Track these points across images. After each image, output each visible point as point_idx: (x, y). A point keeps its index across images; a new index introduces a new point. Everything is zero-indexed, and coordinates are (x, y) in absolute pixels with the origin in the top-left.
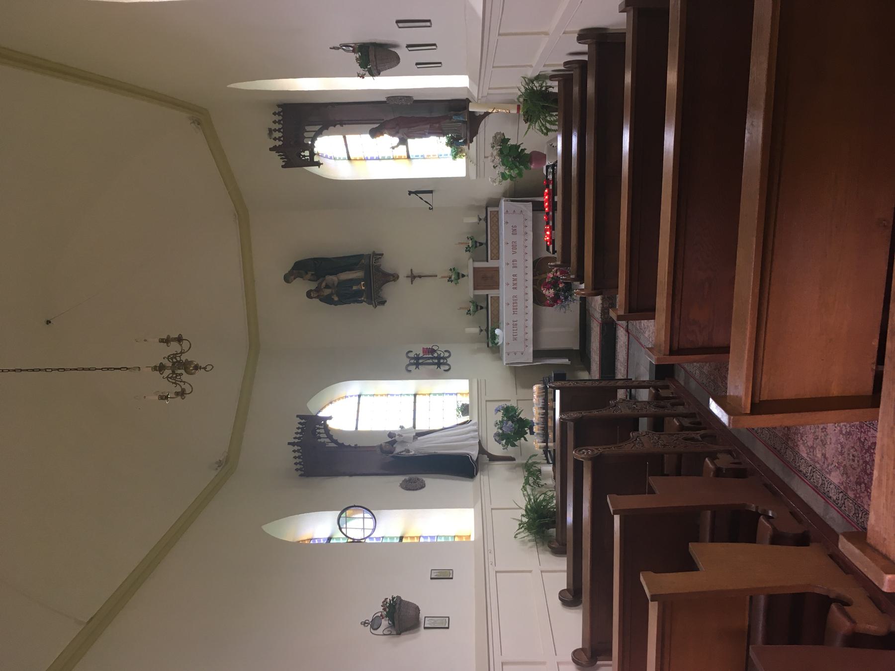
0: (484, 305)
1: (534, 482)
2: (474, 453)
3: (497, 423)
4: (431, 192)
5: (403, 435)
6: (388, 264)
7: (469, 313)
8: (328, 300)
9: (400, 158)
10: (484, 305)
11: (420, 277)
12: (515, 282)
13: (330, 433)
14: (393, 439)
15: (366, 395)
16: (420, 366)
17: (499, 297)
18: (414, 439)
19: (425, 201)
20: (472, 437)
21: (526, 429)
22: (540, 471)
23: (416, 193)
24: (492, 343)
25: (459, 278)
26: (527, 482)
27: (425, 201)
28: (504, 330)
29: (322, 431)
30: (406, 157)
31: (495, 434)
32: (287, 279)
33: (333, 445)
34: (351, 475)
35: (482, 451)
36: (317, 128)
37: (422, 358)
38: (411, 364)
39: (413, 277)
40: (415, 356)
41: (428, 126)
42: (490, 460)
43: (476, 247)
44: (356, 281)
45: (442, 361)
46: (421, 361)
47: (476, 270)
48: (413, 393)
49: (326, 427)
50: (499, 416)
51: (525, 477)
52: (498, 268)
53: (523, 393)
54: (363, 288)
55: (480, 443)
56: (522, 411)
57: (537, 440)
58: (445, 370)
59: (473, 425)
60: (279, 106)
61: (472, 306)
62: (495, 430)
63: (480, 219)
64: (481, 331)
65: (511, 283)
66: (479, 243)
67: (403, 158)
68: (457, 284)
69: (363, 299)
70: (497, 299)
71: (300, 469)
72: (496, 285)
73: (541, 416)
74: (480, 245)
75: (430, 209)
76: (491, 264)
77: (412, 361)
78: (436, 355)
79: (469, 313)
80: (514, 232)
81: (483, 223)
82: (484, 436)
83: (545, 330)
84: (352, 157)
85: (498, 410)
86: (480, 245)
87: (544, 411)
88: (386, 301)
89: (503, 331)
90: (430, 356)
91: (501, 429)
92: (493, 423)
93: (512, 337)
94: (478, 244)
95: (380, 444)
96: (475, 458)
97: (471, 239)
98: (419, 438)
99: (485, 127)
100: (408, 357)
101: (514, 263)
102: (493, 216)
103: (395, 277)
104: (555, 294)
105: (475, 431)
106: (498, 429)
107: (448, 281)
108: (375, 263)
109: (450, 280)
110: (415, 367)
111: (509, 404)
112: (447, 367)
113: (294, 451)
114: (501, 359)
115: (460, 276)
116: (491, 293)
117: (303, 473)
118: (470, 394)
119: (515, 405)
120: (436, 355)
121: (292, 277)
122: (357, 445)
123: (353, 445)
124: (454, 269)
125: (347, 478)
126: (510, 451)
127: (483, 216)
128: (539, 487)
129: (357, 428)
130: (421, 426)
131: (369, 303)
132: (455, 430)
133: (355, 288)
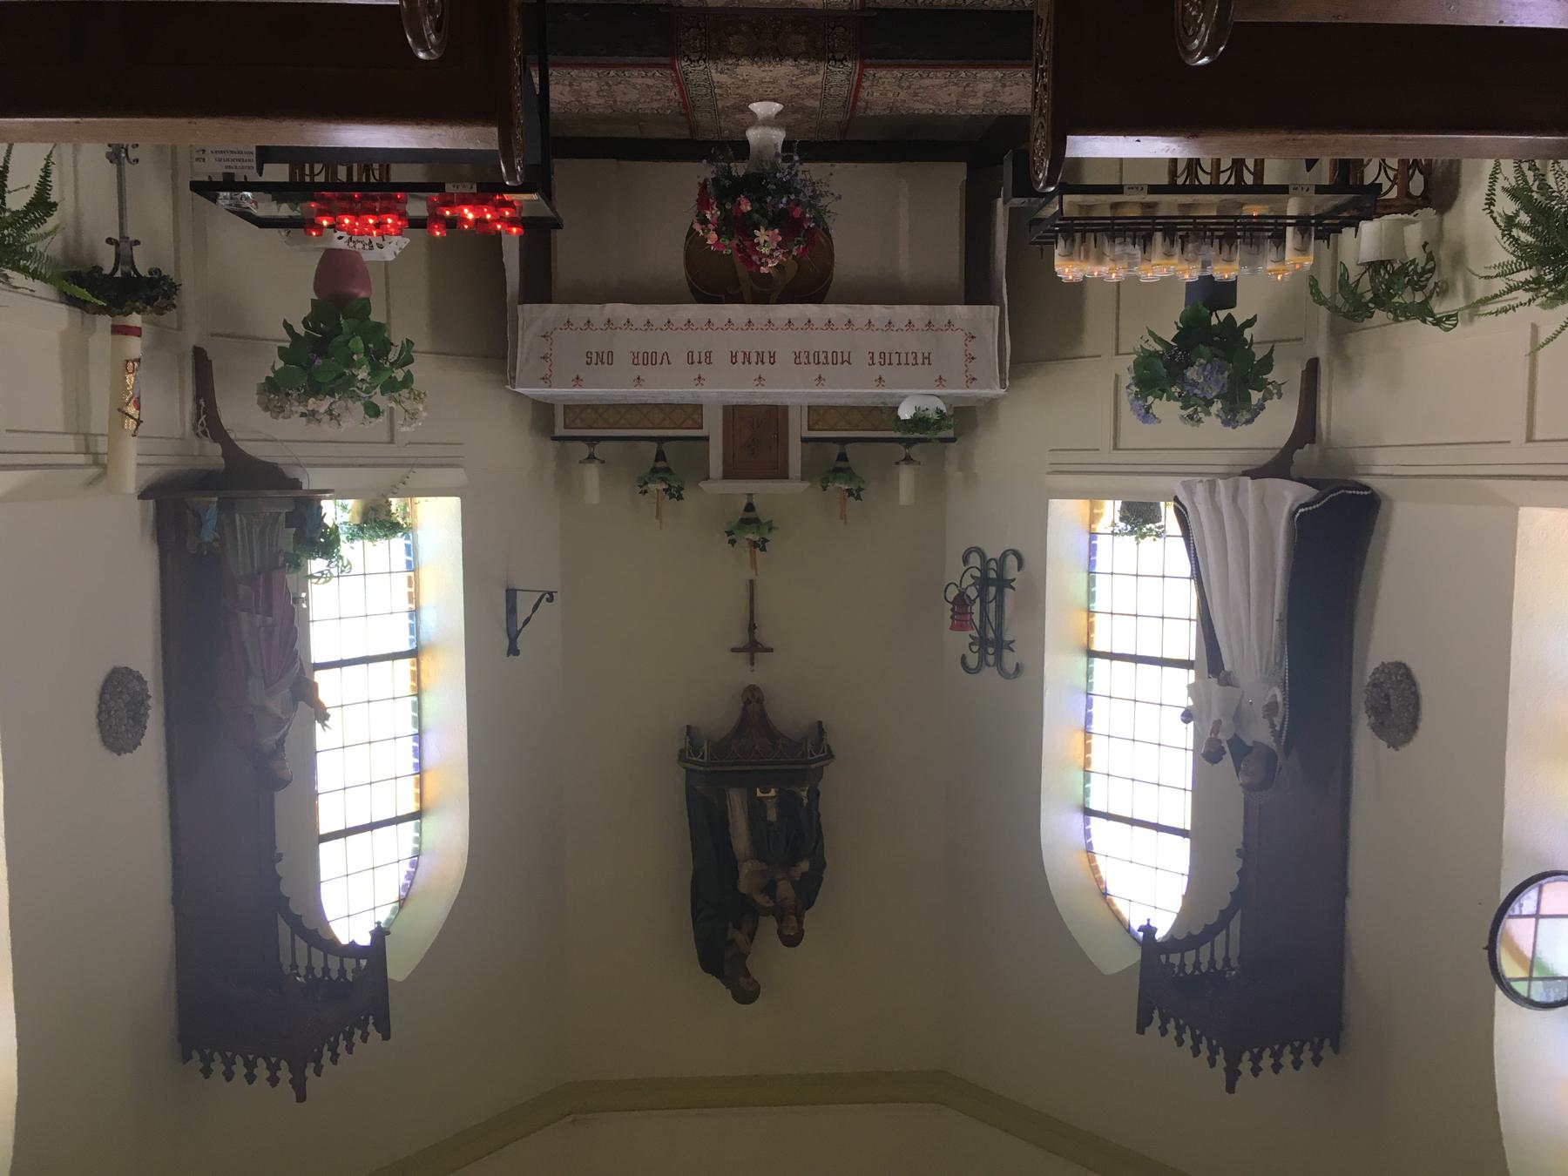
0: (835, 449)
1: (1417, 286)
2: (1290, 494)
3: (1191, 417)
4: (511, 594)
5: (1215, 717)
6: (718, 715)
7: (855, 494)
8: (808, 890)
9: (417, 676)
10: (835, 449)
11: (752, 628)
12: (754, 359)
13: (1196, 932)
14: (1227, 749)
15: (1086, 792)
16: (1007, 638)
17: (809, 407)
18: (1228, 684)
19: (533, 611)
20: (1234, 500)
21: (1214, 321)
22: (1374, 267)
23: (513, 637)
24: (939, 429)
25: (757, 521)
26: (1422, 312)
27: (533, 611)
28: (906, 391)
29: (1190, 957)
30: (414, 659)
31: (1226, 423)
32: (746, 994)
33: (1235, 924)
34: (1344, 892)
35: (1278, 467)
36: (284, 929)
37: (982, 631)
38: (999, 662)
39: (753, 648)
40: (975, 648)
41: (243, 615)
42: (1312, 442)
43: (667, 470)
44: (755, 809)
45: (993, 575)
46: (991, 635)
47: (728, 475)
48: (1084, 659)
49: (1172, 943)
50: (1167, 409)
51: (1396, 320)
52: (726, 408)
53: (1097, 328)
54: (773, 793)
55: (1256, 473)
56: (1151, 333)
57: (1270, 266)
58: (1020, 567)
59: (1191, 491)
60: (186, 1058)
61: (837, 485)
62: (1212, 422)
63: (591, 458)
64: (908, 459)
65: (755, 370)
66: (656, 460)
67: (415, 669)
68: (774, 524)
69: (804, 794)
70: (817, 414)
71: (1317, 1049)
72: (775, 416)
73: (1177, 250)
74: (664, 459)
75: (551, 600)
76: (713, 427)
77: (991, 659)
78: (972, 593)
79: (855, 494)
80: (604, 358)
81: (599, 449)
82: (1226, 458)
83: (906, 267)
84: (412, 807)
85: (1147, 415)
86: (664, 459)
87: (1158, 236)
88: (820, 723)
89: (905, 397)
90: (976, 608)
91: (1210, 403)
92: (1188, 428)
93: (910, 367)
94: (661, 464)
95: (1241, 789)
96: (1309, 492)
97: (646, 483)
98: (1227, 667)
99: (276, 440)
100: (978, 670)
101: (696, 358)
102: (578, 421)
103: (753, 697)
104: (771, 225)
105: (1212, 490)
106: (1208, 414)
107: (763, 549)
108: (702, 757)
109: (761, 545)
110: (1006, 654)
111: (1127, 378)
112: (1012, 561)
113: (1256, 1071)
114: (991, 403)
115: (750, 519)
116: (798, 428)
117: (1327, 1042)
118: (1095, 496)
119: (1130, 361)
120: (972, 593)
121: (742, 981)
122: (1238, 850)
123: (1238, 864)
124: (729, 533)
125: (1349, 903)
126: (1287, 373)
127: (584, 449)
128: (1432, 271)
129: (1182, 833)
130: (1184, 643)
131: (819, 774)
132: (1205, 557)
133: (772, 815)
